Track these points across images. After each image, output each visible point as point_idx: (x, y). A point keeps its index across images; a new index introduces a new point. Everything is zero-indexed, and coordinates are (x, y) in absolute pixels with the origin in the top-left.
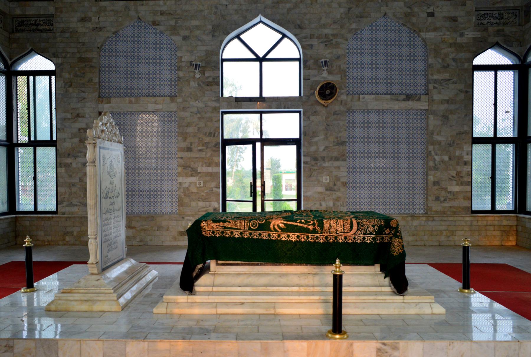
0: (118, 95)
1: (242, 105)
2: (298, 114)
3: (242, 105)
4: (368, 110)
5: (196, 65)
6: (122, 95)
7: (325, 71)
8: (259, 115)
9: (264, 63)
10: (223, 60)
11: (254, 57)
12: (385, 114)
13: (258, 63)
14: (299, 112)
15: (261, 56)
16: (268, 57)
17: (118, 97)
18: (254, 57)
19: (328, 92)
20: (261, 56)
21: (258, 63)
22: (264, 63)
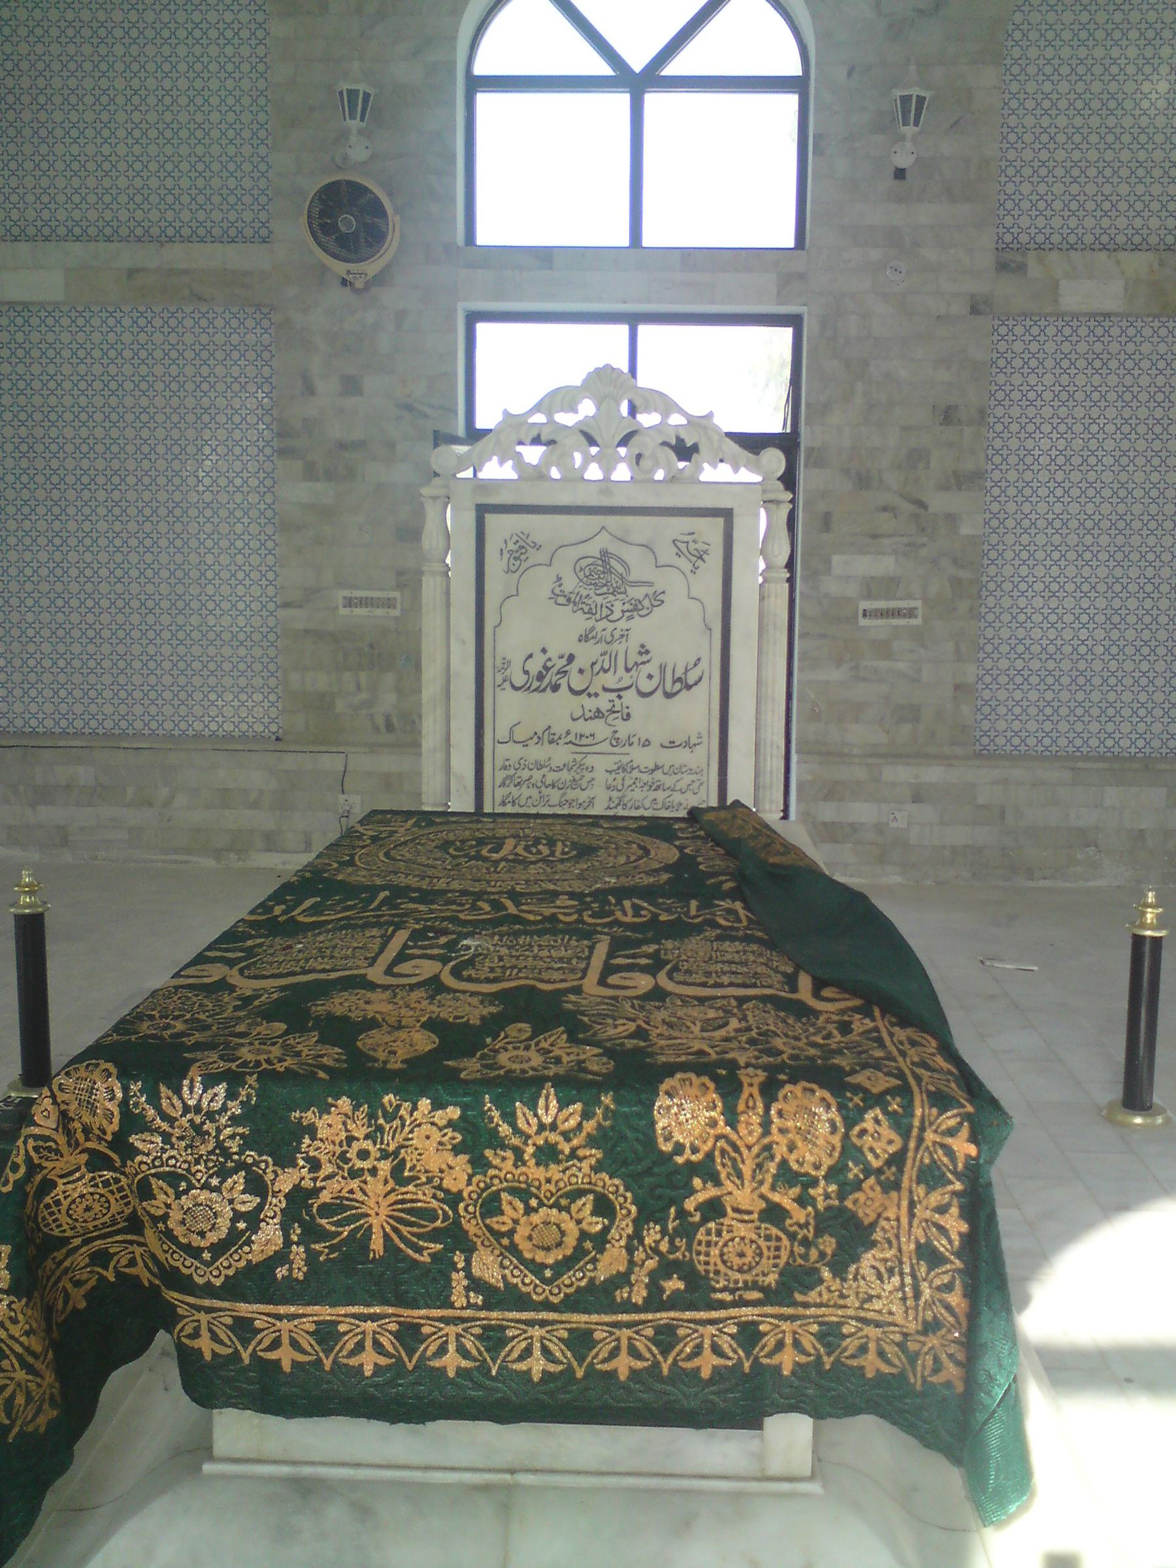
0: (201, 232)
1: (549, 283)
2: (482, 328)
3: (549, 283)
4: (1060, 315)
5: (353, 94)
6: (155, 231)
7: (909, 145)
8: (623, 330)
9: (652, 100)
10: (477, 84)
11: (606, 70)
12: (142, 322)
13: (622, 100)
14: (793, 321)
15: (637, 62)
16: (672, 69)
17: (139, 240)
18: (606, 70)
19: (347, 223)
20: (637, 62)
21: (622, 100)
22: (652, 100)
